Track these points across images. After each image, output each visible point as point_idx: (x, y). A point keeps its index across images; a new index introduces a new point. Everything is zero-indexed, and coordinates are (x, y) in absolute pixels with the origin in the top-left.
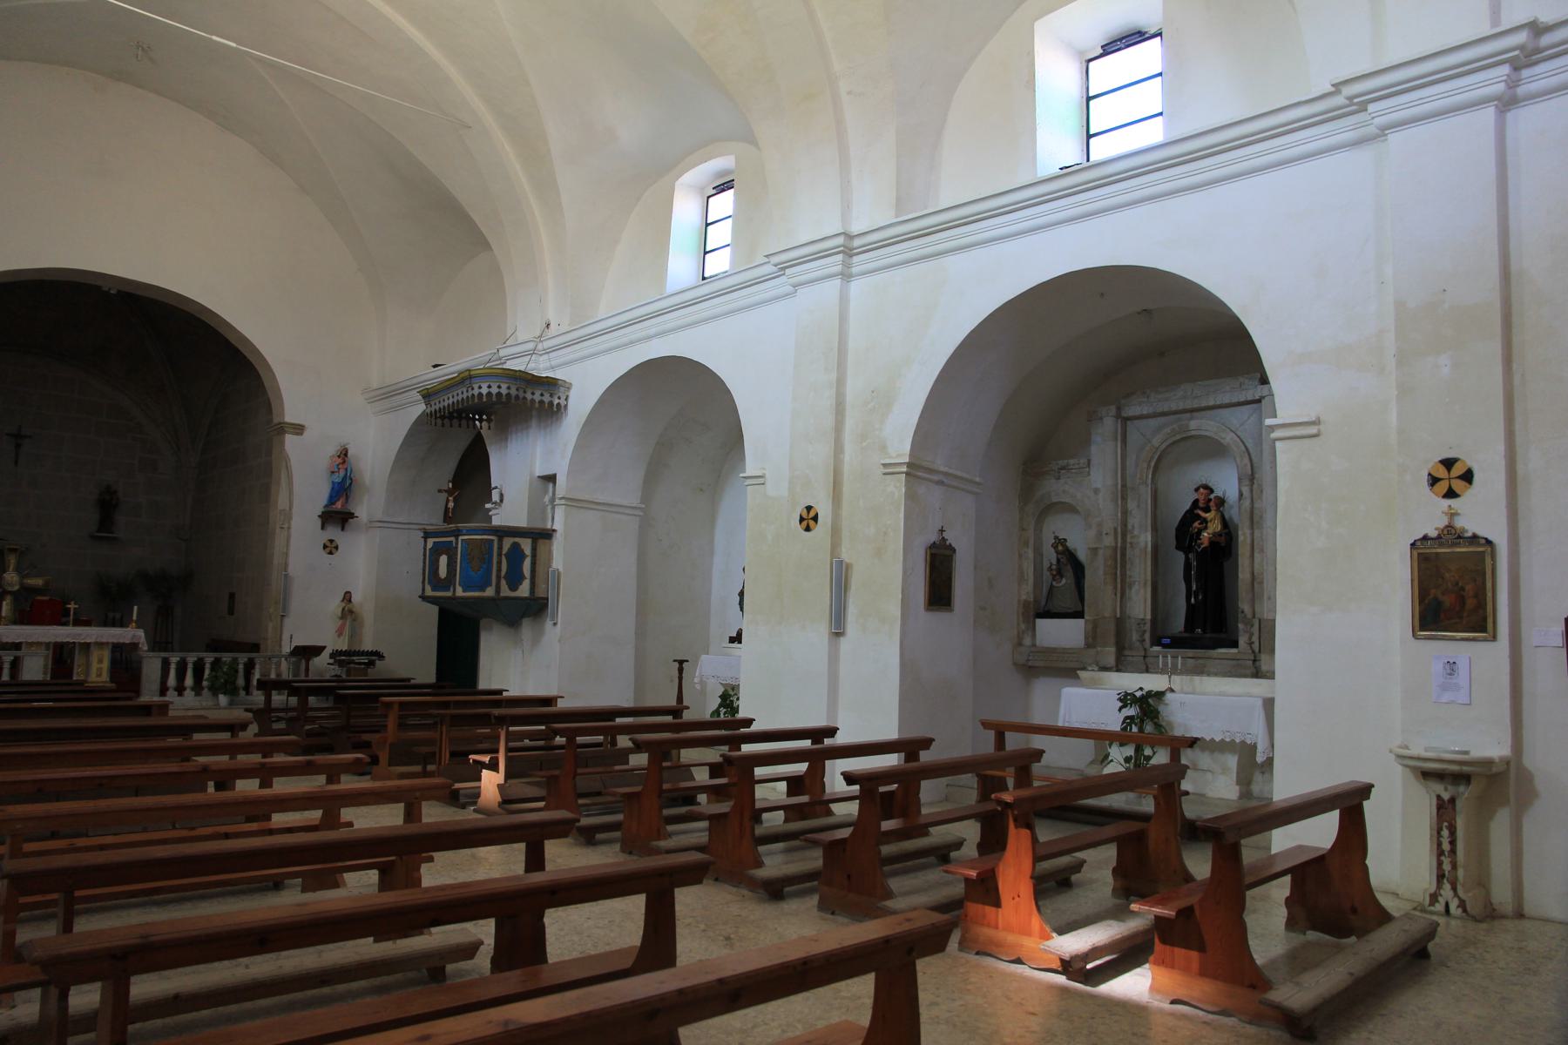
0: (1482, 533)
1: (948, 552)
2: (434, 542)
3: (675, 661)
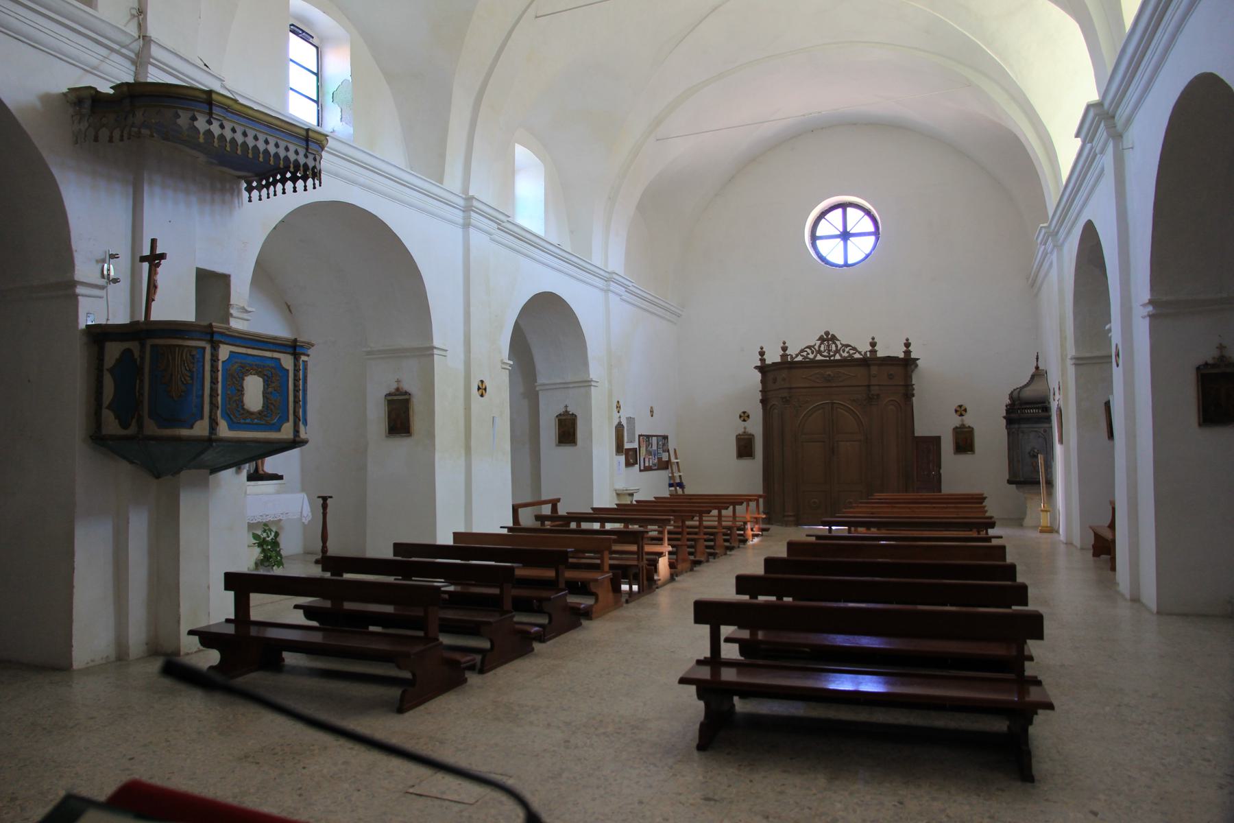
1: (407, 397)
2: (288, 370)
3: (319, 497)
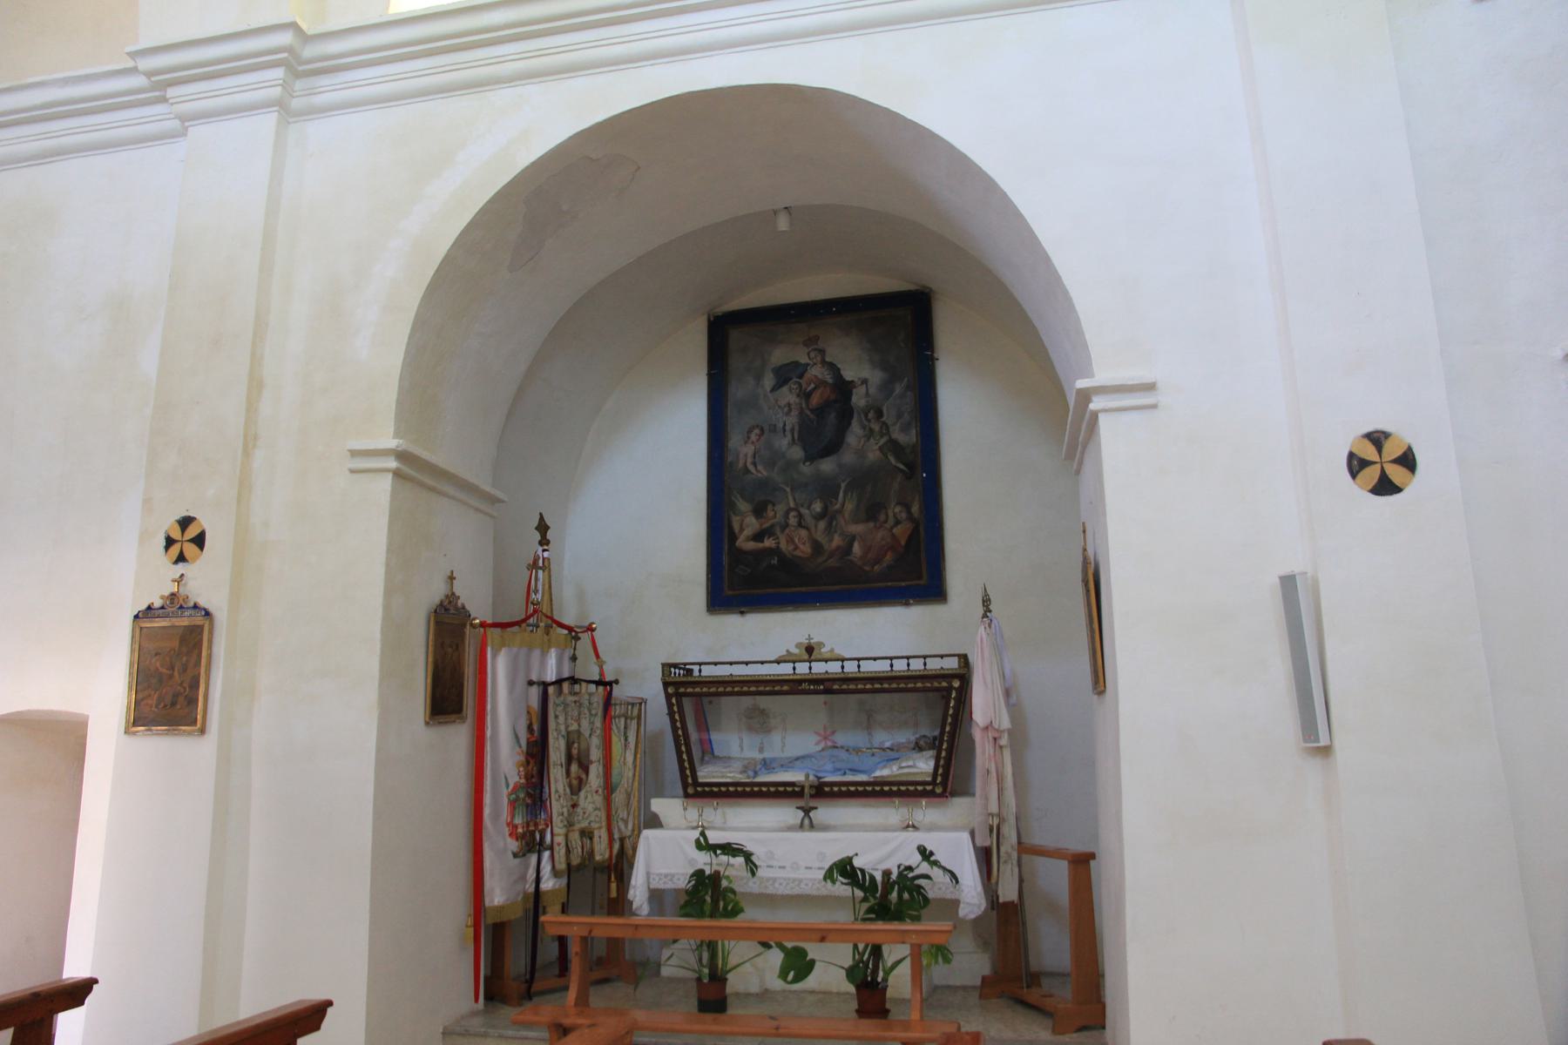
0: (203, 603)
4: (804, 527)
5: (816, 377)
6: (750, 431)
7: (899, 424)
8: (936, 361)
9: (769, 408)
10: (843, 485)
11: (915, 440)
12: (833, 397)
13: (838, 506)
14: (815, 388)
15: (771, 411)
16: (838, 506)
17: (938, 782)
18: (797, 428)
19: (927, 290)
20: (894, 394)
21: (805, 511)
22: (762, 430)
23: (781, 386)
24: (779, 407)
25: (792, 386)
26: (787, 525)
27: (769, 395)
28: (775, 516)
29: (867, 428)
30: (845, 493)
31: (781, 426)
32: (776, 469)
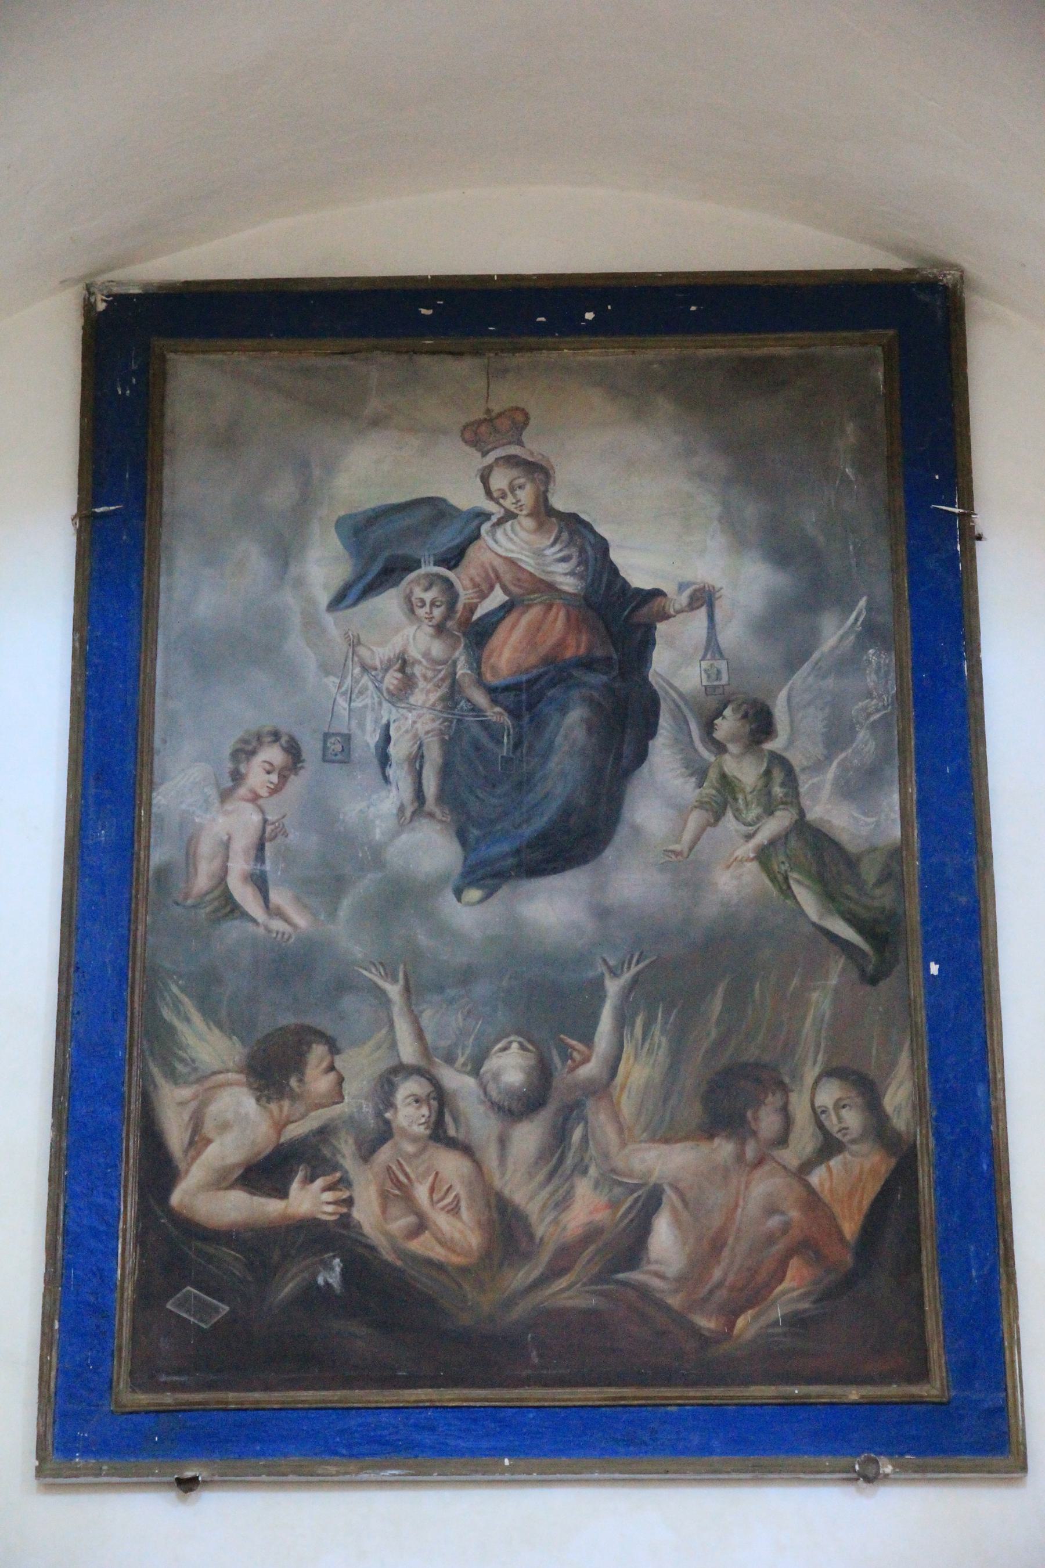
4: (452, 1144)
5: (512, 562)
6: (244, 752)
7: (832, 772)
8: (978, 544)
9: (326, 669)
10: (613, 987)
11: (897, 832)
12: (577, 647)
13: (590, 1070)
14: (506, 609)
15: (332, 681)
16: (590, 1070)
17: (864, 599)
18: (434, 755)
19: (949, 279)
20: (816, 656)
21: (456, 1080)
22: (294, 752)
23: (372, 588)
24: (365, 668)
25: (418, 593)
26: (385, 1133)
27: (329, 620)
28: (337, 1094)
29: (713, 775)
30: (622, 1021)
31: (372, 738)
32: (346, 904)
